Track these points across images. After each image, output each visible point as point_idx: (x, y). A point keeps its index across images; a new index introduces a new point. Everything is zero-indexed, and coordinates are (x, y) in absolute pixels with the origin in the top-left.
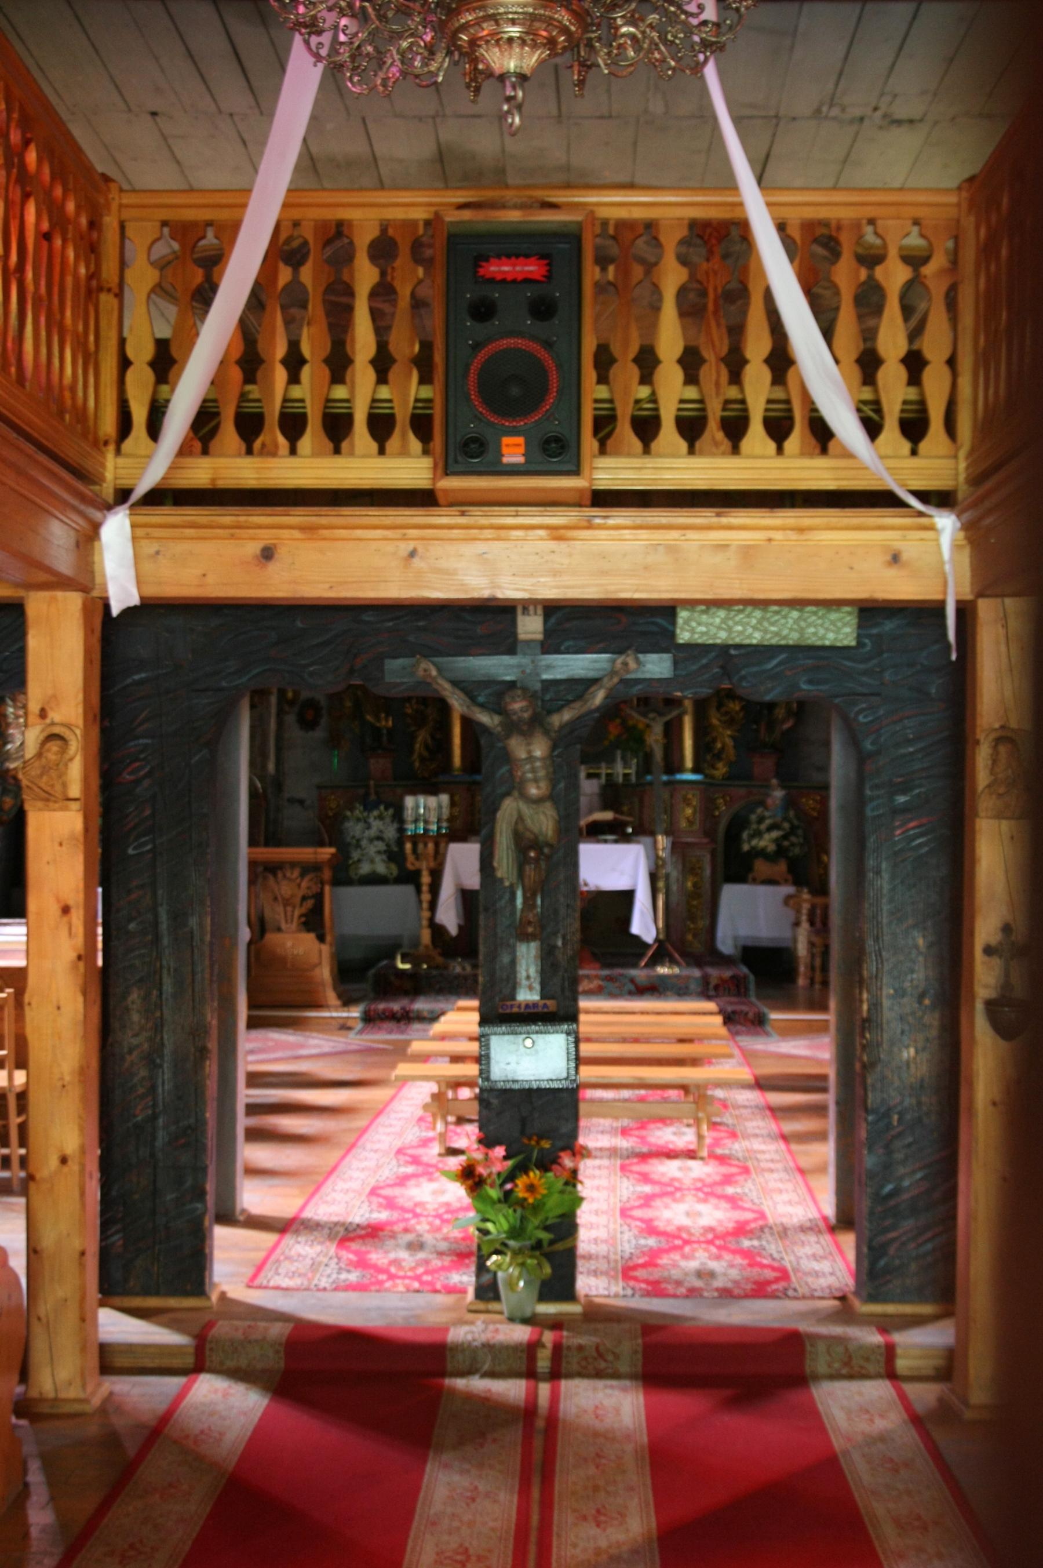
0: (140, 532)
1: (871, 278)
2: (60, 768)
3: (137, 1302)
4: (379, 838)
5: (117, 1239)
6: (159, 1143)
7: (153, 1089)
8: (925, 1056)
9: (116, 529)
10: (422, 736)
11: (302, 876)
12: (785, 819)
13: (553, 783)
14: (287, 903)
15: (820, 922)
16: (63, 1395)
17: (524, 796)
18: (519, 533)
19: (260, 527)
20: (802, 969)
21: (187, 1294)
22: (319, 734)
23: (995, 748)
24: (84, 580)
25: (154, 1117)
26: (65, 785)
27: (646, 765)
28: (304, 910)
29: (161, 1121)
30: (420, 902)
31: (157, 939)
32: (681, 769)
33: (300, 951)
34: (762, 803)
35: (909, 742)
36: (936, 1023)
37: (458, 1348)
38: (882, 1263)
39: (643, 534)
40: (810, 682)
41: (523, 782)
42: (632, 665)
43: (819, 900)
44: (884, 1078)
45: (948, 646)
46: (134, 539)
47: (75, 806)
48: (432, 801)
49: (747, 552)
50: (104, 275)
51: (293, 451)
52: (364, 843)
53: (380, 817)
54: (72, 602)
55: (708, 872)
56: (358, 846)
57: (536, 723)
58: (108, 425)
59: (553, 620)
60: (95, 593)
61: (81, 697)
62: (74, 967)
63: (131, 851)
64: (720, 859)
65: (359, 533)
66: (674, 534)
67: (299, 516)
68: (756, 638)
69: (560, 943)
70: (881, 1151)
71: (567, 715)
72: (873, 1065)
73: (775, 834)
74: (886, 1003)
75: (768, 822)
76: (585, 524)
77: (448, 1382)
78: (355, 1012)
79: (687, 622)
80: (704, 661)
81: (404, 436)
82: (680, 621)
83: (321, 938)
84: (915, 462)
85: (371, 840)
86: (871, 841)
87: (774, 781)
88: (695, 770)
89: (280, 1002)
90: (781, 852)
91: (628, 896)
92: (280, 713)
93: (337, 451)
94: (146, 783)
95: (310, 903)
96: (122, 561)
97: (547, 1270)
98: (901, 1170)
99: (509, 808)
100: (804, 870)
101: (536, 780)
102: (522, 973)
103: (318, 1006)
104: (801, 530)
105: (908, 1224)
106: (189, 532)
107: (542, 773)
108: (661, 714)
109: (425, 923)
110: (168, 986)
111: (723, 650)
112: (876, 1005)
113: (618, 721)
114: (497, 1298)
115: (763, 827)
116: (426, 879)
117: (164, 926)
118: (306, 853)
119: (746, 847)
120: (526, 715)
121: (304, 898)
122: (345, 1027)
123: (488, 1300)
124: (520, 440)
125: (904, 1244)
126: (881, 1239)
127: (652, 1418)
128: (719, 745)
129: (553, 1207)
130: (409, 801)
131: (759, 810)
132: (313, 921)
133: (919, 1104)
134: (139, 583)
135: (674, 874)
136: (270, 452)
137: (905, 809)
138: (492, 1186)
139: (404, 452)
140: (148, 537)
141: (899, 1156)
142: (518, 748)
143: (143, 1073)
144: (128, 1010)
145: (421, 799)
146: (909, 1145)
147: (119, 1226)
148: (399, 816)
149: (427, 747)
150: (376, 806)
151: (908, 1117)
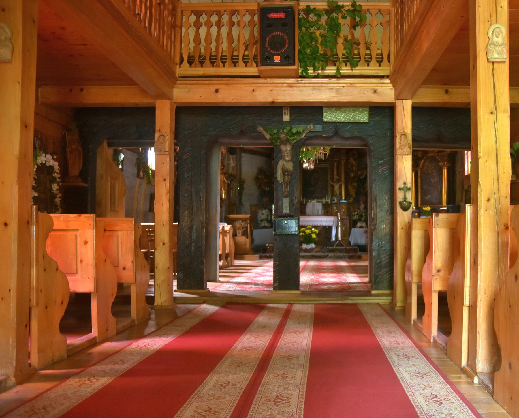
1: (398, 98)
6: (192, 250)
11: (242, 222)
18: (280, 85)
19: (214, 84)
21: (200, 289)
23: (401, 137)
26: (164, 148)
35: (383, 147)
39: (311, 85)
40: (357, 132)
41: (284, 156)
42: (312, 128)
47: (167, 153)
50: (177, 23)
51: (224, 66)
54: (167, 102)
55: (348, 225)
57: (287, 141)
58: (178, 60)
59: (292, 117)
62: (167, 194)
66: (319, 85)
67: (224, 81)
68: (343, 120)
74: (378, 214)
81: (252, 62)
84: (380, 68)
88: (345, 200)
93: (235, 66)
95: (244, 229)
98: (382, 256)
99: (281, 163)
101: (287, 156)
102: (284, 205)
105: (384, 270)
107: (289, 154)
110: (195, 210)
111: (336, 123)
112: (375, 214)
121: (243, 228)
124: (279, 57)
125: (383, 275)
136: (218, 66)
137: (382, 164)
139: (252, 66)
141: (381, 253)
142: (283, 148)
143: (188, 232)
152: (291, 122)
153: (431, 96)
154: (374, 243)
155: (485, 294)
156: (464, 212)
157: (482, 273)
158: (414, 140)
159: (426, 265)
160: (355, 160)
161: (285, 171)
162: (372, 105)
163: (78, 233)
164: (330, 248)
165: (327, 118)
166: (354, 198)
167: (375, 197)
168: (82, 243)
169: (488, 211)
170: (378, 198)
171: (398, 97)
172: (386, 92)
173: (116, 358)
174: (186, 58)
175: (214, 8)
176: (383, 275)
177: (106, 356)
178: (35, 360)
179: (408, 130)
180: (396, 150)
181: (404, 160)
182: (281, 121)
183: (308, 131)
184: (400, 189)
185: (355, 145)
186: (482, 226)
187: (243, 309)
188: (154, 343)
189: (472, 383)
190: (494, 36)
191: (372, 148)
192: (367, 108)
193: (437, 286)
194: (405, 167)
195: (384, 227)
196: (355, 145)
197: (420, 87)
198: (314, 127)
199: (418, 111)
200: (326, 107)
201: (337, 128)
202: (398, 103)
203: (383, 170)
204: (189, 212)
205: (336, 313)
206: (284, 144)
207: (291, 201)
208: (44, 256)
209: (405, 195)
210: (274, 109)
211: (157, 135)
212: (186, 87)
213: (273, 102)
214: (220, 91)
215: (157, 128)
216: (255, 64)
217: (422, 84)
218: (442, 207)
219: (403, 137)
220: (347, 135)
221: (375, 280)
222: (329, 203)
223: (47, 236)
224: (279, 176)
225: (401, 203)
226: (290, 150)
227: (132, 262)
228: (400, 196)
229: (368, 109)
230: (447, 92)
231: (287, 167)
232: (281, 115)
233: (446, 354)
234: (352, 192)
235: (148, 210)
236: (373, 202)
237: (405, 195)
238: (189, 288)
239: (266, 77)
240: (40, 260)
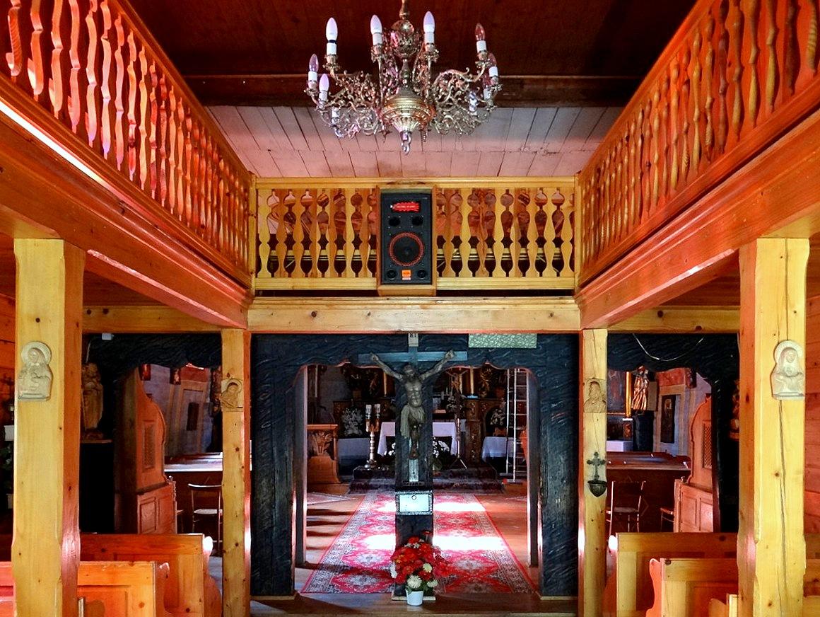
18: (410, 306)
23: (590, 386)
32: (470, 394)
35: (556, 384)
38: (549, 580)
39: (456, 306)
42: (452, 356)
49: (495, 313)
51: (323, 276)
57: (416, 378)
58: (253, 266)
67: (326, 300)
71: (428, 375)
74: (549, 482)
88: (474, 395)
94: (268, 401)
99: (406, 410)
101: (416, 399)
110: (277, 477)
112: (545, 483)
121: (326, 443)
124: (409, 271)
125: (558, 573)
137: (555, 409)
139: (366, 276)
142: (409, 387)
143: (267, 510)
164: (454, 470)
172: (566, 316)
174: (264, 262)
175: (306, 187)
184: (589, 462)
190: (785, 360)
202: (587, 335)
206: (410, 382)
207: (421, 464)
212: (268, 308)
215: (225, 372)
216: (370, 273)
219: (594, 386)
227: (200, 601)
228: (588, 473)
235: (185, 428)
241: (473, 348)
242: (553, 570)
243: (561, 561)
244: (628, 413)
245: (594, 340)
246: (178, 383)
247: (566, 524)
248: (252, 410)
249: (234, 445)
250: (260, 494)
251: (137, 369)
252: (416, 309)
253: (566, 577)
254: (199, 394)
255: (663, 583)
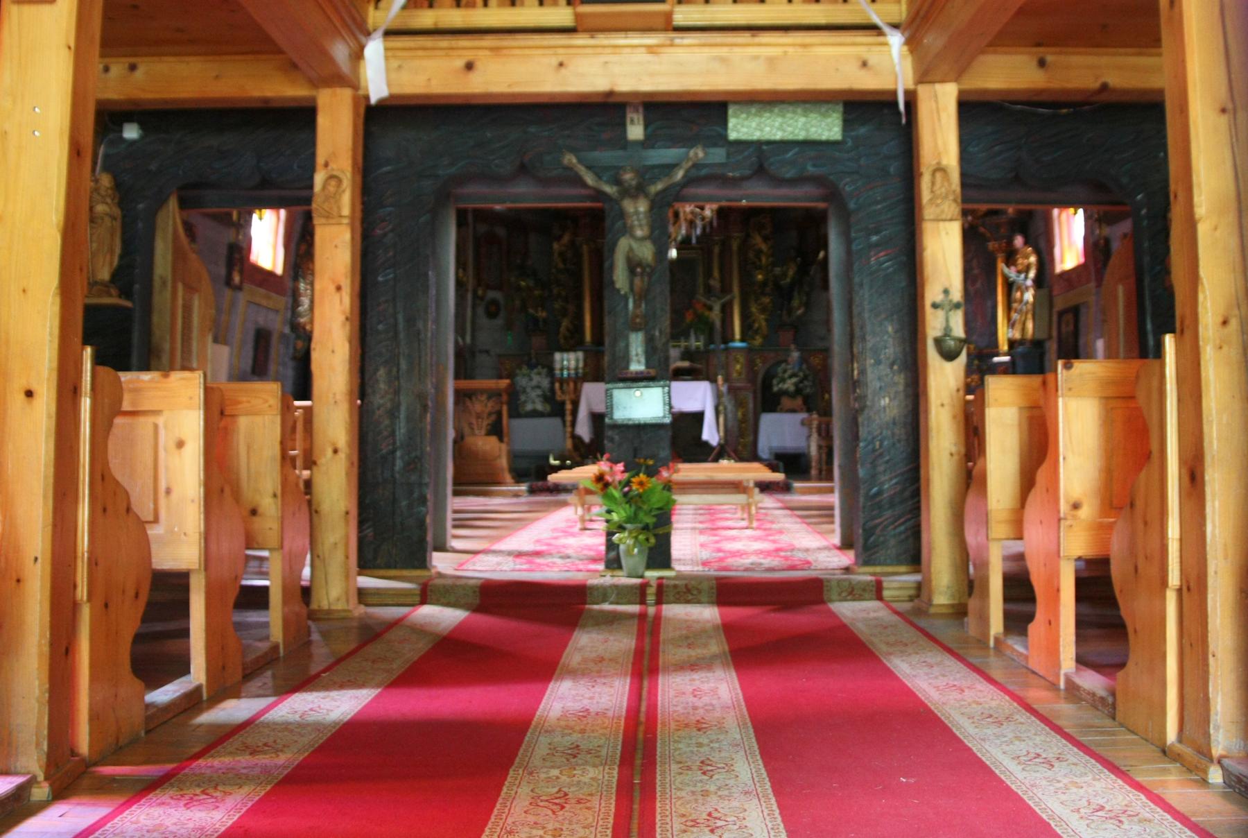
0: (390, 54)
2: (336, 196)
3: (382, 572)
4: (538, 387)
5: (369, 532)
6: (397, 468)
7: (393, 434)
8: (896, 403)
9: (374, 49)
10: (565, 323)
12: (801, 369)
13: (652, 228)
14: (478, 416)
15: (826, 434)
16: (334, 607)
17: (633, 236)
18: (628, 50)
20: (814, 464)
22: (499, 321)
24: (351, 82)
25: (393, 452)
26: (339, 208)
27: (710, 340)
28: (490, 421)
29: (398, 454)
30: (565, 432)
31: (396, 333)
32: (733, 340)
33: (487, 447)
34: (786, 361)
35: (878, 203)
36: (902, 381)
37: (594, 588)
38: (872, 539)
39: (706, 50)
40: (814, 166)
41: (632, 227)
43: (825, 419)
44: (869, 418)
45: (899, 113)
46: (387, 58)
48: (572, 356)
49: (771, 61)
52: (528, 390)
53: (539, 374)
54: (346, 94)
55: (751, 405)
56: (524, 391)
57: (638, 191)
59: (650, 129)
60: (361, 92)
61: (350, 153)
62: (344, 325)
63: (380, 279)
64: (759, 395)
65: (527, 52)
66: (725, 49)
67: (489, 41)
68: (778, 136)
69: (657, 333)
70: (869, 466)
71: (659, 186)
72: (862, 409)
73: (794, 380)
74: (869, 370)
75: (789, 372)
76: (668, 42)
77: (587, 606)
78: (523, 487)
79: (735, 126)
80: (746, 154)
82: (730, 125)
83: (501, 440)
85: (533, 388)
86: (856, 267)
87: (793, 347)
88: (742, 340)
89: (474, 478)
90: (798, 391)
91: (698, 417)
92: (474, 307)
94: (391, 235)
95: (493, 417)
96: (379, 72)
97: (653, 540)
98: (883, 478)
99: (623, 244)
100: (813, 399)
101: (641, 226)
102: (633, 352)
103: (499, 483)
104: (804, 46)
105: (888, 513)
106: (420, 53)
107: (644, 222)
108: (719, 298)
109: (568, 435)
110: (404, 365)
111: (759, 144)
112: (863, 372)
113: (691, 311)
114: (620, 567)
115: (786, 375)
116: (569, 407)
117: (401, 326)
118: (491, 384)
119: (775, 389)
120: (634, 183)
121: (490, 414)
122: (516, 495)
123: (614, 569)
125: (886, 527)
126: (871, 524)
127: (721, 615)
128: (756, 325)
129: (656, 500)
130: (558, 356)
131: (783, 365)
132: (496, 430)
133: (893, 434)
134: (389, 85)
135: (730, 407)
137: (877, 245)
138: (615, 488)
140: (394, 57)
141: (881, 469)
142: (628, 206)
143: (387, 422)
144: (377, 381)
145: (565, 355)
146: (887, 462)
147: (370, 523)
148: (551, 370)
149: (568, 330)
150: (535, 366)
151: (886, 443)
152: (649, 142)
153: (1008, 73)
154: (861, 444)
155: (1226, 558)
156: (1159, 353)
157: (1217, 504)
158: (964, 185)
159: (971, 499)
160: (765, 239)
161: (633, 266)
162: (851, 98)
163: (160, 421)
165: (738, 131)
166: (765, 337)
167: (862, 328)
168: (172, 445)
169: (1225, 348)
170: (868, 328)
171: (925, 75)
172: (889, 64)
173: (248, 737)
176: (888, 522)
177: (226, 735)
178: (83, 744)
179: (951, 158)
180: (921, 208)
181: (943, 233)
182: (622, 142)
183: (690, 163)
184: (935, 306)
185: (796, 199)
186: (1212, 388)
187: (541, 613)
188: (338, 705)
189: (1204, 782)
191: (852, 205)
192: (837, 104)
193: (1076, 544)
194: (944, 250)
195: (886, 405)
196: (796, 199)
197: (983, 52)
198: (706, 154)
199: (972, 110)
200: (736, 103)
201: (762, 157)
202: (923, 92)
203: (883, 261)
204: (390, 372)
205: (772, 622)
208: (101, 475)
209: (947, 320)
210: (604, 111)
211: (319, 178)
213: (611, 94)
214: (479, 65)
215: (320, 160)
217: (990, 45)
218: (998, 355)
220: (790, 173)
221: (866, 540)
222: (702, 348)
223: (110, 425)
224: (620, 277)
225: (938, 342)
226: (645, 213)
228: (934, 324)
229: (840, 108)
230: (1042, 63)
231: (640, 255)
232: (623, 126)
233: (1114, 719)
234: (761, 320)
235: (249, 369)
236: (856, 341)
237: (947, 320)
238: (388, 566)
239: (593, 31)
240: (94, 484)
241: (739, 143)
242: (877, 521)
243: (892, 505)
244: (1004, 347)
245: (936, 102)
246: (239, 288)
247: (899, 441)
248: (364, 221)
249: (333, 281)
250: (374, 392)
251: (94, 769)
252: (642, 56)
253: (900, 533)
254: (271, 316)
255: (1060, 400)
